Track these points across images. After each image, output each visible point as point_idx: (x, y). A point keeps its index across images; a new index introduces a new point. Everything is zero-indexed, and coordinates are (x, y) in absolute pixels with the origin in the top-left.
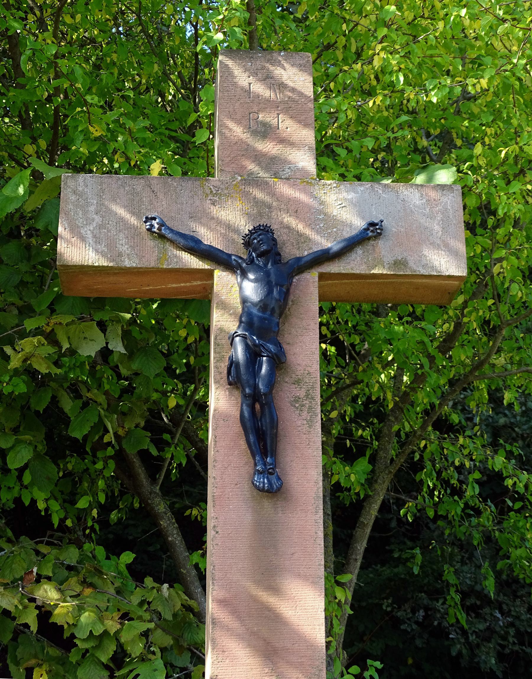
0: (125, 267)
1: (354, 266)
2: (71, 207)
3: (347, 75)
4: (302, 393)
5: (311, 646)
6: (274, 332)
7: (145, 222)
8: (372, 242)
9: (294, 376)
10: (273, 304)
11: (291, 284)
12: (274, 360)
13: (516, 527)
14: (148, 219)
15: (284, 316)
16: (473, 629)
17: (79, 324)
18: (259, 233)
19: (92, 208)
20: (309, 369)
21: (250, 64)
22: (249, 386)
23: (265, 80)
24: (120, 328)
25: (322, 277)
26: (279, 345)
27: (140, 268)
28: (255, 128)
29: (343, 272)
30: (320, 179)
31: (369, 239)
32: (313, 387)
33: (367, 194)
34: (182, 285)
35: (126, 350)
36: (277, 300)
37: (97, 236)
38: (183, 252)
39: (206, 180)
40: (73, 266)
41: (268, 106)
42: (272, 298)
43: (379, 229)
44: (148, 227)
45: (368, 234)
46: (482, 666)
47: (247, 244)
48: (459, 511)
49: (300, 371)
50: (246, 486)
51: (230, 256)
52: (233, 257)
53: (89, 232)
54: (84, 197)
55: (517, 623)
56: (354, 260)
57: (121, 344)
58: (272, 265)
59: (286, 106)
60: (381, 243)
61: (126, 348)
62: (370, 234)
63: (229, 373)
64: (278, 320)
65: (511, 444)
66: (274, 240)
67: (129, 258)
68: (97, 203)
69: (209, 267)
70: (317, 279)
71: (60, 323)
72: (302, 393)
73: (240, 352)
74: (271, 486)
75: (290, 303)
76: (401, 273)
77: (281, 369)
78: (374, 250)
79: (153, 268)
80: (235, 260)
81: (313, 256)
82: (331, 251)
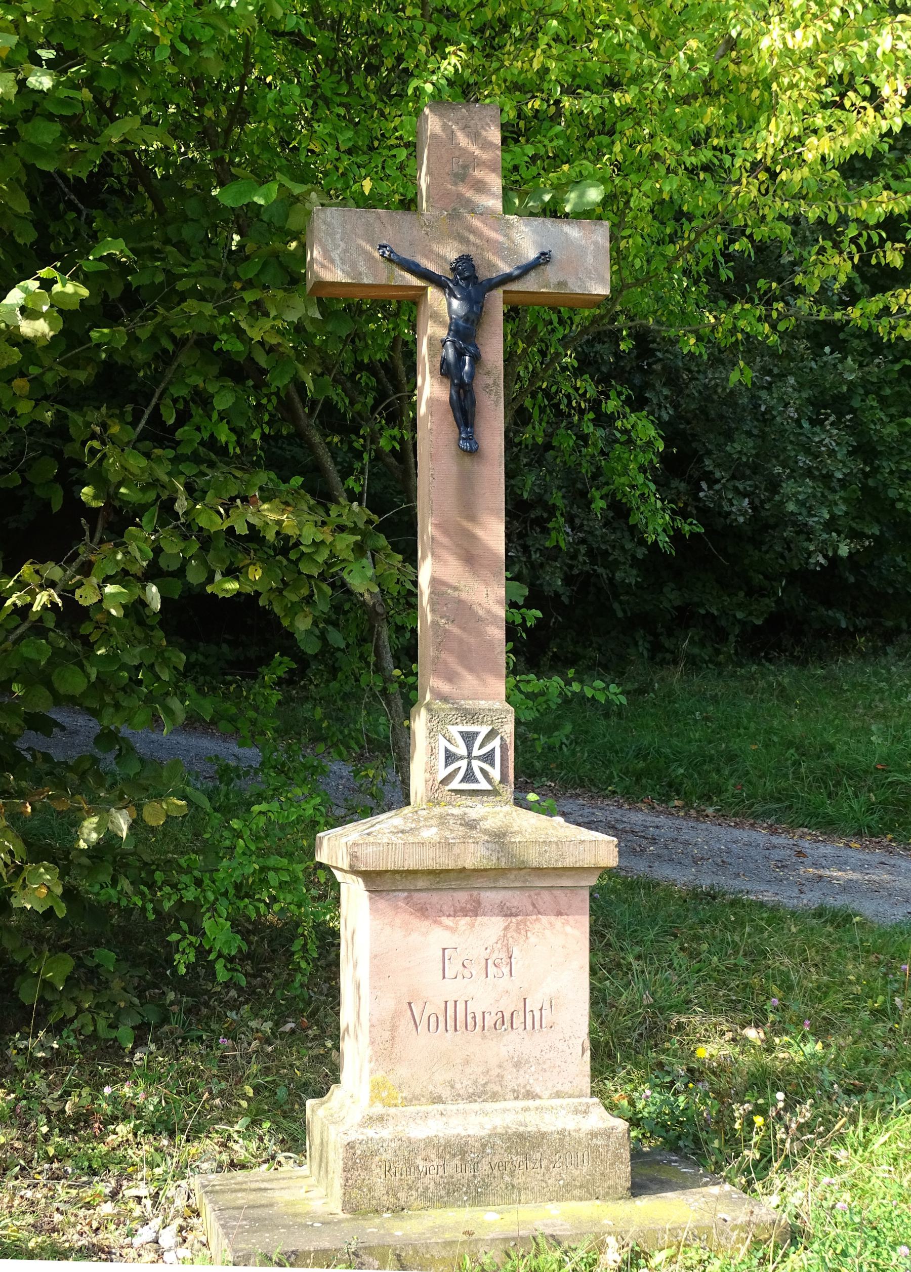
4: (491, 382)
5: (495, 555)
13: (619, 459)
14: (381, 247)
16: (537, 546)
19: (338, 236)
25: (504, 292)
41: (456, 144)
46: (546, 588)
48: (571, 443)
49: (489, 365)
50: (453, 447)
55: (590, 538)
63: (442, 367)
65: (622, 385)
66: (473, 266)
72: (491, 382)
73: (451, 353)
74: (470, 448)
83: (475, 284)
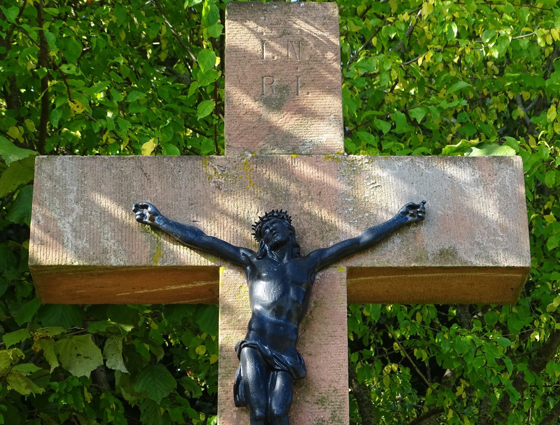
0: (111, 266)
1: (390, 257)
2: (46, 195)
3: (393, 28)
4: (327, 415)
6: (291, 340)
7: (135, 211)
8: (412, 229)
9: (316, 394)
10: (289, 306)
11: (312, 283)
12: (291, 374)
15: (304, 321)
17: (71, 338)
18: (272, 220)
19: (72, 196)
20: (335, 385)
21: (263, 18)
22: (260, 407)
23: (280, 37)
24: (121, 342)
25: (352, 272)
26: (297, 357)
27: (129, 267)
28: (269, 95)
29: (377, 265)
30: (349, 154)
31: (409, 224)
32: (340, 407)
33: (406, 171)
34: (183, 286)
35: (128, 369)
36: (294, 302)
37: (78, 229)
38: (182, 247)
39: (210, 159)
40: (48, 266)
42: (288, 299)
43: (420, 212)
44: (137, 217)
45: (407, 219)
47: (259, 235)
49: (324, 387)
51: (237, 249)
52: (242, 251)
53: (67, 225)
54: (61, 184)
56: (390, 251)
57: (121, 362)
58: (288, 259)
59: (307, 66)
60: (423, 229)
61: (127, 366)
62: (410, 219)
64: (296, 326)
66: (291, 229)
67: (115, 256)
68: (78, 190)
69: (213, 264)
70: (345, 275)
71: (47, 338)
72: (327, 415)
75: (313, 305)
76: (449, 265)
77: (301, 386)
78: (415, 238)
79: (145, 266)
80: (244, 254)
81: (339, 247)
82: (362, 241)
83: (292, 256)
